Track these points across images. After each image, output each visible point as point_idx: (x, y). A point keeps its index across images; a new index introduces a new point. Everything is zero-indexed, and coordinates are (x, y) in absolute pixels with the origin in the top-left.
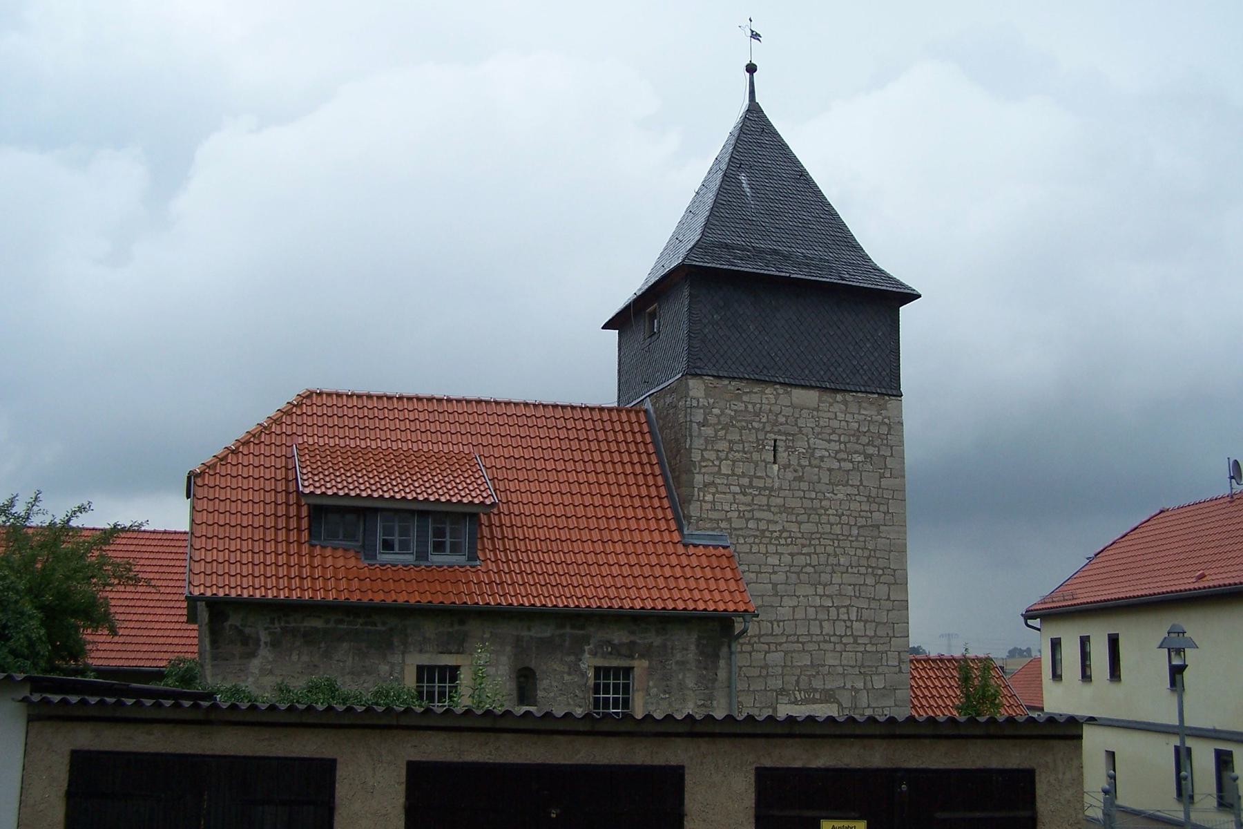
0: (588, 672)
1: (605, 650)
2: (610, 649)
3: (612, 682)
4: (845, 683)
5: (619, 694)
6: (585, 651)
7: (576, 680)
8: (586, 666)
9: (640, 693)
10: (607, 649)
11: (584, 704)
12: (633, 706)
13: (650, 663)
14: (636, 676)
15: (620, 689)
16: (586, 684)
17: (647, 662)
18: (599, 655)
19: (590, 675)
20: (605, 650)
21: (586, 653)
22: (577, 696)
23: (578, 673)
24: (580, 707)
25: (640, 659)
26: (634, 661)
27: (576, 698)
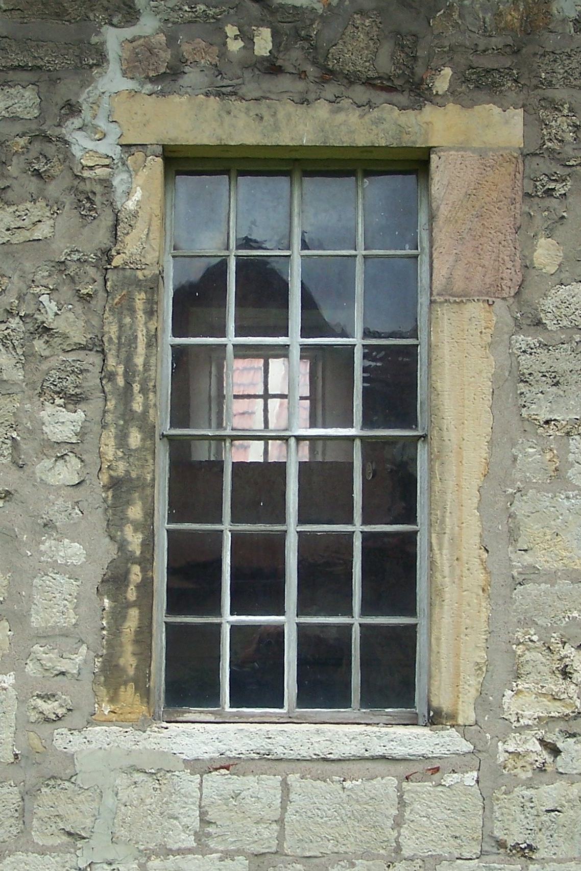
0: (119, 181)
1: (235, 46)
2: (264, 43)
3: (358, 527)
4: (101, 383)
5: (234, 629)
6: (102, 59)
7: (40, 232)
8: (109, 147)
9: (475, 309)
10: (248, 38)
11: (92, 380)
12: (433, 411)
13: (534, 121)
14: (443, 212)
15: (187, 625)
16: (107, 254)
17: (517, 116)
18: (192, 77)
19: (131, 205)
20: (235, 46)
21: (113, 68)
22: (45, 330)
23: (53, 189)
24: (74, 400)
25: (468, 105)
26: (429, 113)
27: (39, 345)
